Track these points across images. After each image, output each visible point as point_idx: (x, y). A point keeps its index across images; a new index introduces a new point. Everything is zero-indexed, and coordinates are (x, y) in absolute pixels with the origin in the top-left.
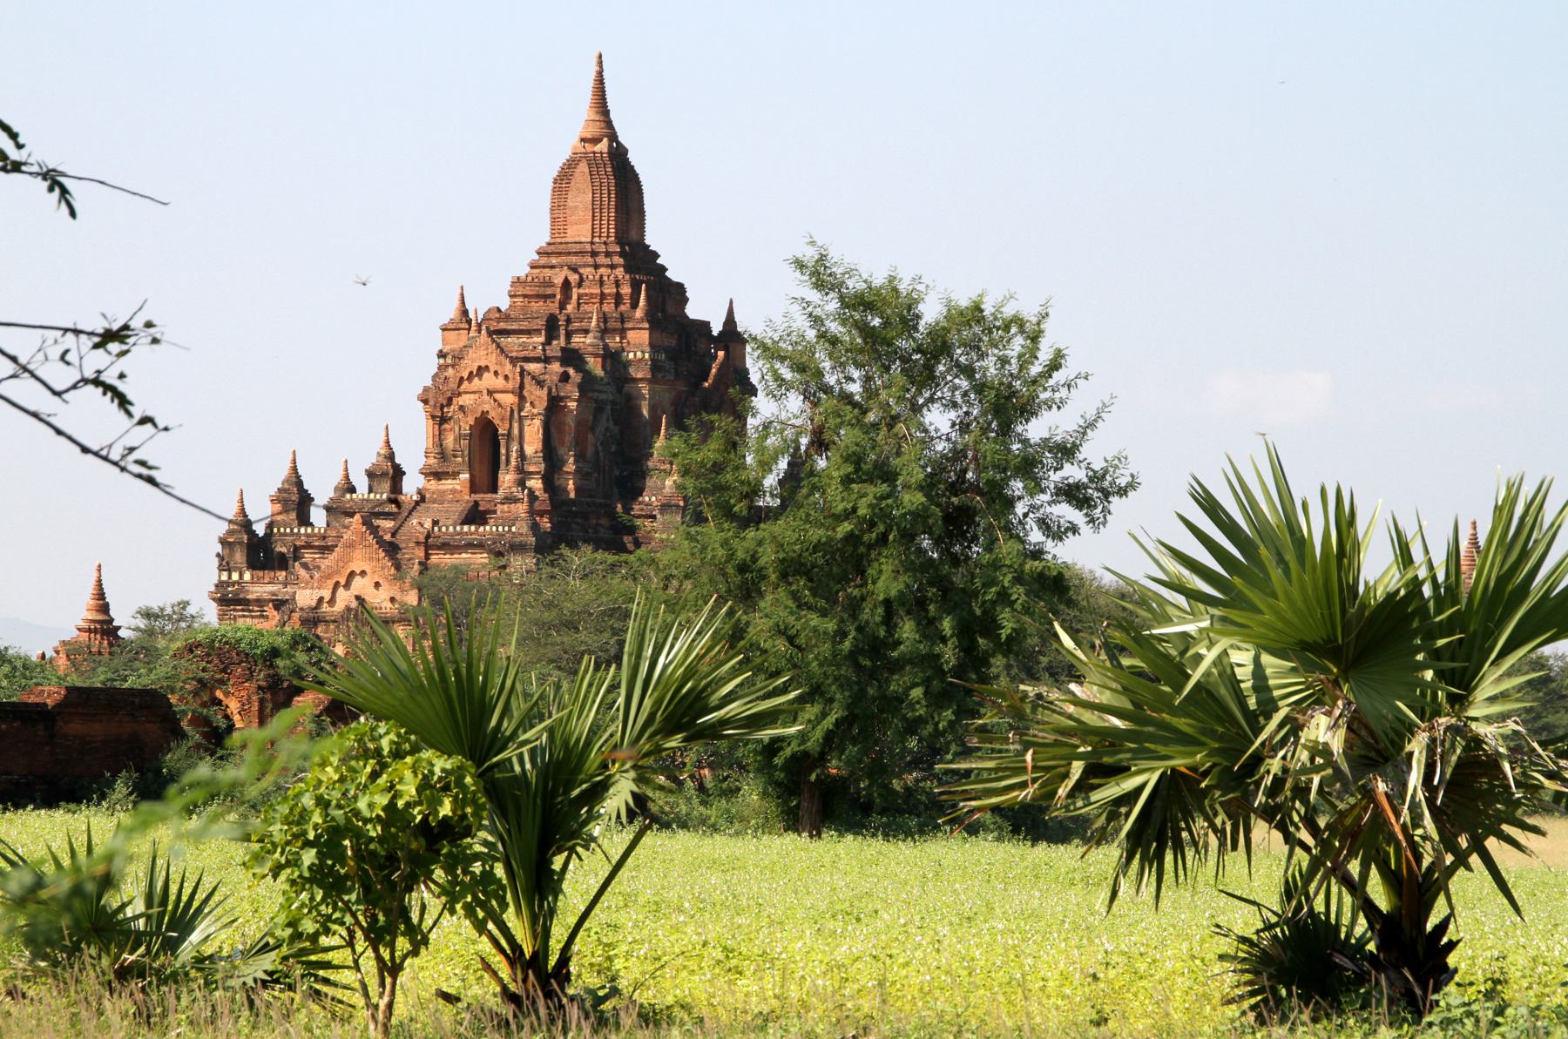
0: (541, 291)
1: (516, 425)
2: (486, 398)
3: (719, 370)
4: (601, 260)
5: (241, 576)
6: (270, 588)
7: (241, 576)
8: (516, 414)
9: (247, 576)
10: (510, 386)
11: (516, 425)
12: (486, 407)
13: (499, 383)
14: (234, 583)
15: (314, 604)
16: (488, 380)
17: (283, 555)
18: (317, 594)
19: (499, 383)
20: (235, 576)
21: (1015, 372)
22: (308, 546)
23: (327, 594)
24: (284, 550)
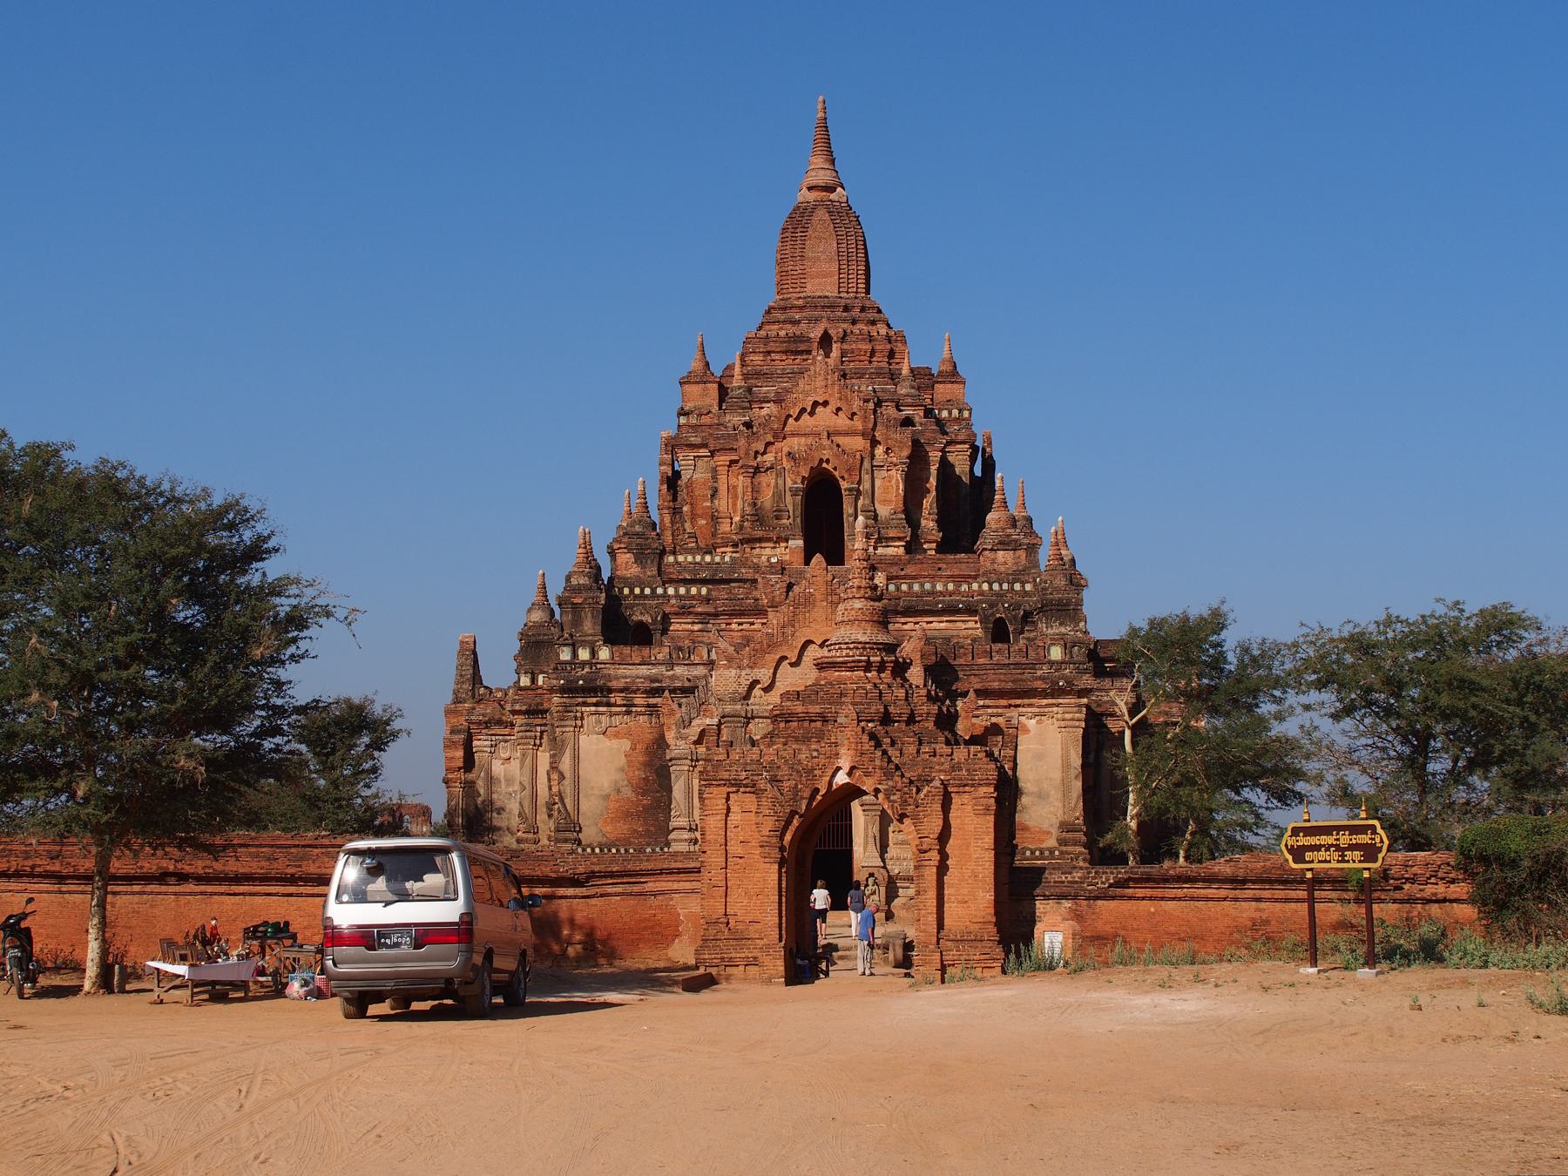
0: (792, 347)
1: (866, 478)
2: (826, 442)
3: (941, 523)
4: (856, 312)
5: (593, 653)
6: (644, 670)
7: (593, 653)
8: (865, 463)
9: (604, 654)
10: (858, 424)
11: (866, 478)
12: (826, 454)
13: (842, 421)
14: (584, 664)
15: (743, 690)
16: (824, 417)
17: (641, 624)
18: (746, 677)
19: (842, 421)
20: (584, 654)
21: (961, 727)
22: (684, 612)
23: (764, 675)
24: (647, 619)
